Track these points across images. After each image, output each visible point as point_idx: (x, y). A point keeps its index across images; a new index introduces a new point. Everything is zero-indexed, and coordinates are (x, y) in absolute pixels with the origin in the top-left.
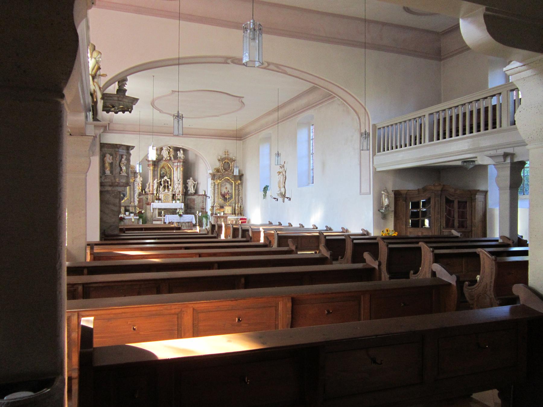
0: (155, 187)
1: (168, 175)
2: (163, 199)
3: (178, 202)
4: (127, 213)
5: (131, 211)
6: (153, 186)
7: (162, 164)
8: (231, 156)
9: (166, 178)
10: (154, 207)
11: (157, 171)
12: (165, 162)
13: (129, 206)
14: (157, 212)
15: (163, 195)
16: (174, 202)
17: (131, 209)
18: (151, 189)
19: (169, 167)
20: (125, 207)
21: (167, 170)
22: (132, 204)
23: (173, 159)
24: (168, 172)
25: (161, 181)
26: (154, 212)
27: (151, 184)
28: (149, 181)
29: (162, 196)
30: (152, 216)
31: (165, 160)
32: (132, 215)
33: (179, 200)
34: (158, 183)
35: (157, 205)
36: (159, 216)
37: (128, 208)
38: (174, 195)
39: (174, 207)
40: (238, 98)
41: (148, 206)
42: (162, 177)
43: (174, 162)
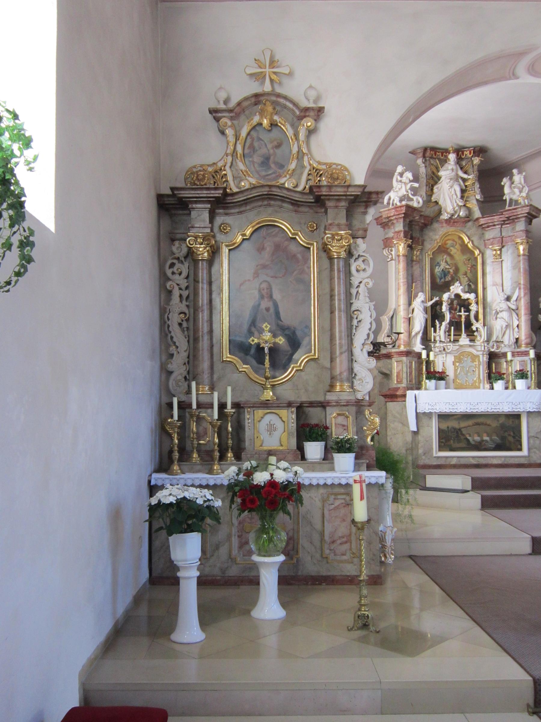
0: (418, 325)
1: (465, 280)
2: (450, 373)
3: (520, 384)
4: (314, 450)
5: (337, 433)
6: (409, 320)
7: (436, 235)
8: (297, 90)
9: (457, 288)
10: (423, 408)
11: (420, 261)
12: (451, 229)
13: (323, 405)
14: (433, 429)
15: (450, 359)
16: (499, 385)
17: (339, 424)
18: (401, 327)
19: (465, 249)
20: (300, 409)
21: (460, 258)
22: (342, 392)
23: (477, 213)
24: (463, 269)
25: (439, 303)
26: (424, 432)
27: (402, 313)
28: (392, 305)
29: (442, 361)
30: (412, 448)
31: (450, 221)
32: (345, 461)
33: (522, 375)
34: (426, 310)
35: (432, 399)
36: (441, 448)
37: (315, 416)
38: (493, 357)
39: (506, 408)
40: (154, 535)
41: (392, 406)
42: (439, 286)
43: (483, 228)
